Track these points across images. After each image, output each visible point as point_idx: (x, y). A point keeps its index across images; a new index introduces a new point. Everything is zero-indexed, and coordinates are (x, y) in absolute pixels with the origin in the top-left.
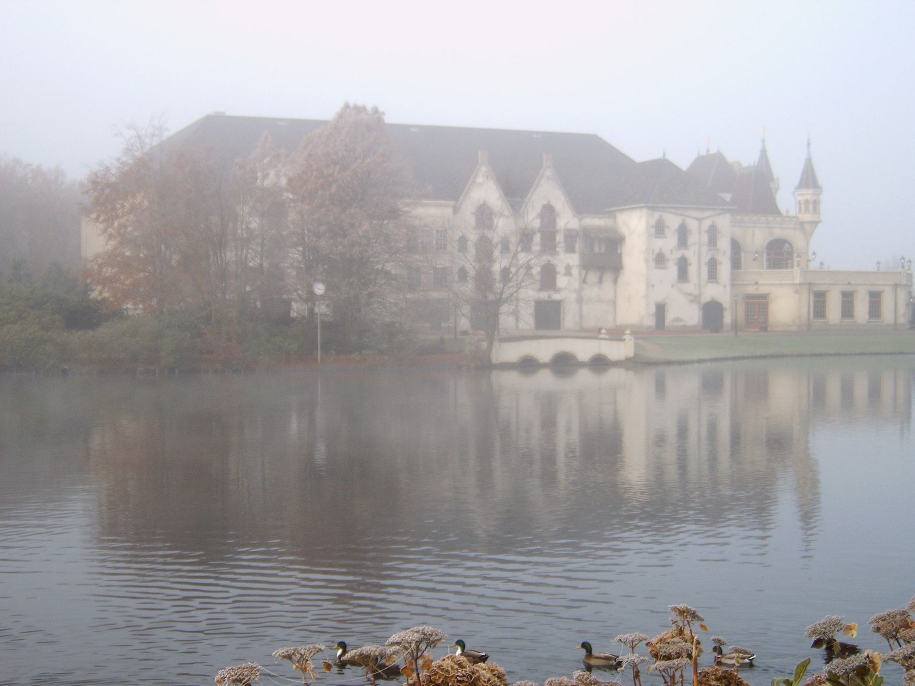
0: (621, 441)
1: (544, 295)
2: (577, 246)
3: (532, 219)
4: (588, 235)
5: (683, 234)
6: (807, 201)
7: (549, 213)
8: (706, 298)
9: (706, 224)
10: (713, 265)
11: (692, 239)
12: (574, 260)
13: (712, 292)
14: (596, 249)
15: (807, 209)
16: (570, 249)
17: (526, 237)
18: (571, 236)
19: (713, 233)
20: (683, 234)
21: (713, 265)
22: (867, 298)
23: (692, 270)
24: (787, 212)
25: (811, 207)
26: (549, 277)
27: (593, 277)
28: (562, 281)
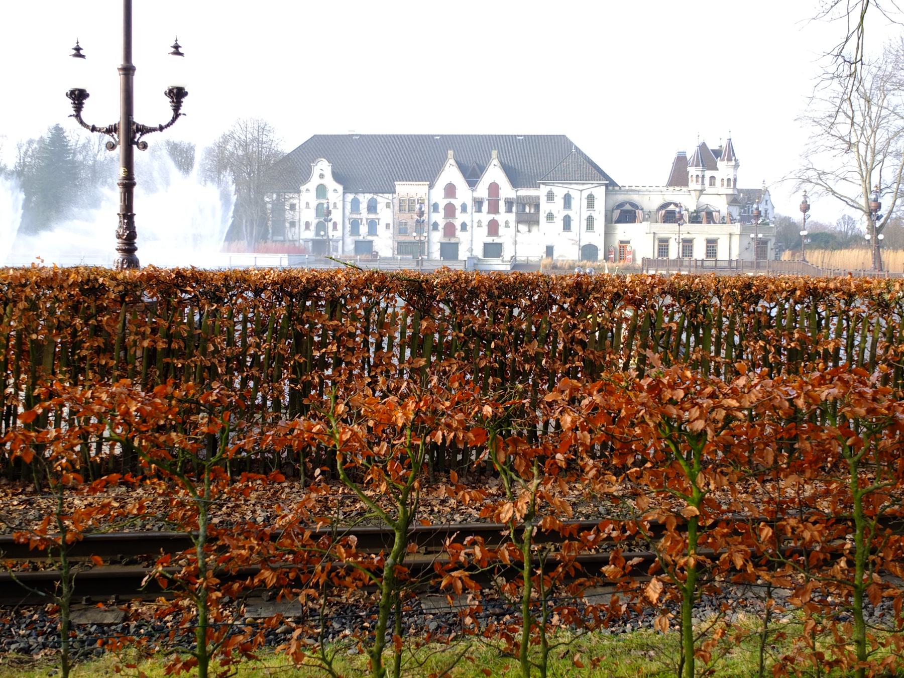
0: (821, 225)
1: (489, 240)
2: (514, 209)
3: (482, 191)
4: (522, 203)
5: (567, 200)
6: (697, 176)
7: (494, 189)
8: (583, 243)
9: (585, 194)
10: (590, 221)
11: (575, 203)
12: (512, 217)
13: (588, 238)
14: (527, 210)
15: (728, 185)
16: (509, 210)
17: (478, 203)
18: (509, 203)
19: (591, 199)
20: (567, 200)
21: (590, 221)
22: (704, 244)
23: (574, 225)
24: (145, 146)
25: (732, 183)
26: (493, 228)
27: (523, 228)
28: (502, 230)
